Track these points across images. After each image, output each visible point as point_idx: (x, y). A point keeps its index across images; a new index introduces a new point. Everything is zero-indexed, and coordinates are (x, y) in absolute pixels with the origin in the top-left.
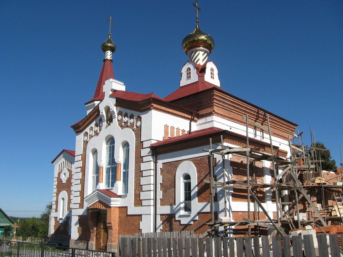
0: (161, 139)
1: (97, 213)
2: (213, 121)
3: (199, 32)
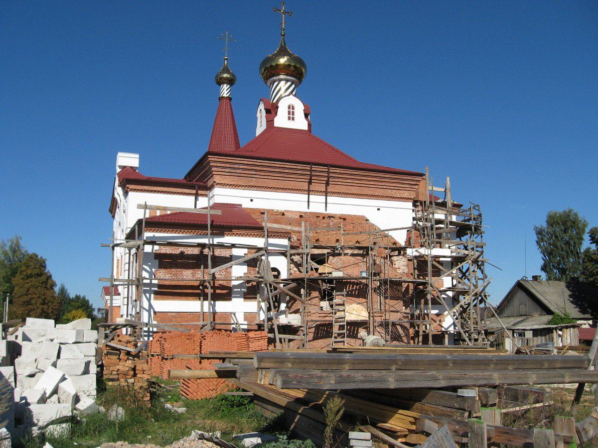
2: (214, 195)
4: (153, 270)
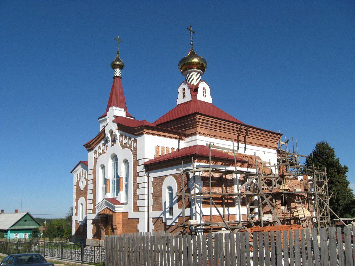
0: (153, 158)
1: (105, 217)
2: (196, 140)
3: (193, 55)
4: (201, 187)
